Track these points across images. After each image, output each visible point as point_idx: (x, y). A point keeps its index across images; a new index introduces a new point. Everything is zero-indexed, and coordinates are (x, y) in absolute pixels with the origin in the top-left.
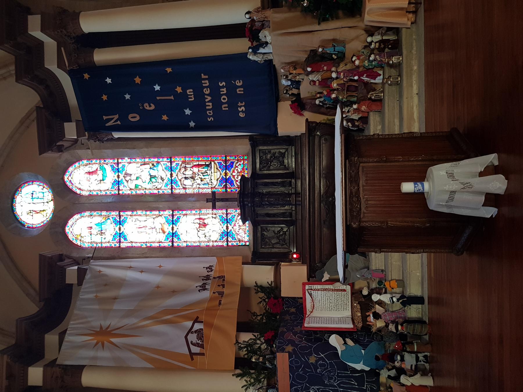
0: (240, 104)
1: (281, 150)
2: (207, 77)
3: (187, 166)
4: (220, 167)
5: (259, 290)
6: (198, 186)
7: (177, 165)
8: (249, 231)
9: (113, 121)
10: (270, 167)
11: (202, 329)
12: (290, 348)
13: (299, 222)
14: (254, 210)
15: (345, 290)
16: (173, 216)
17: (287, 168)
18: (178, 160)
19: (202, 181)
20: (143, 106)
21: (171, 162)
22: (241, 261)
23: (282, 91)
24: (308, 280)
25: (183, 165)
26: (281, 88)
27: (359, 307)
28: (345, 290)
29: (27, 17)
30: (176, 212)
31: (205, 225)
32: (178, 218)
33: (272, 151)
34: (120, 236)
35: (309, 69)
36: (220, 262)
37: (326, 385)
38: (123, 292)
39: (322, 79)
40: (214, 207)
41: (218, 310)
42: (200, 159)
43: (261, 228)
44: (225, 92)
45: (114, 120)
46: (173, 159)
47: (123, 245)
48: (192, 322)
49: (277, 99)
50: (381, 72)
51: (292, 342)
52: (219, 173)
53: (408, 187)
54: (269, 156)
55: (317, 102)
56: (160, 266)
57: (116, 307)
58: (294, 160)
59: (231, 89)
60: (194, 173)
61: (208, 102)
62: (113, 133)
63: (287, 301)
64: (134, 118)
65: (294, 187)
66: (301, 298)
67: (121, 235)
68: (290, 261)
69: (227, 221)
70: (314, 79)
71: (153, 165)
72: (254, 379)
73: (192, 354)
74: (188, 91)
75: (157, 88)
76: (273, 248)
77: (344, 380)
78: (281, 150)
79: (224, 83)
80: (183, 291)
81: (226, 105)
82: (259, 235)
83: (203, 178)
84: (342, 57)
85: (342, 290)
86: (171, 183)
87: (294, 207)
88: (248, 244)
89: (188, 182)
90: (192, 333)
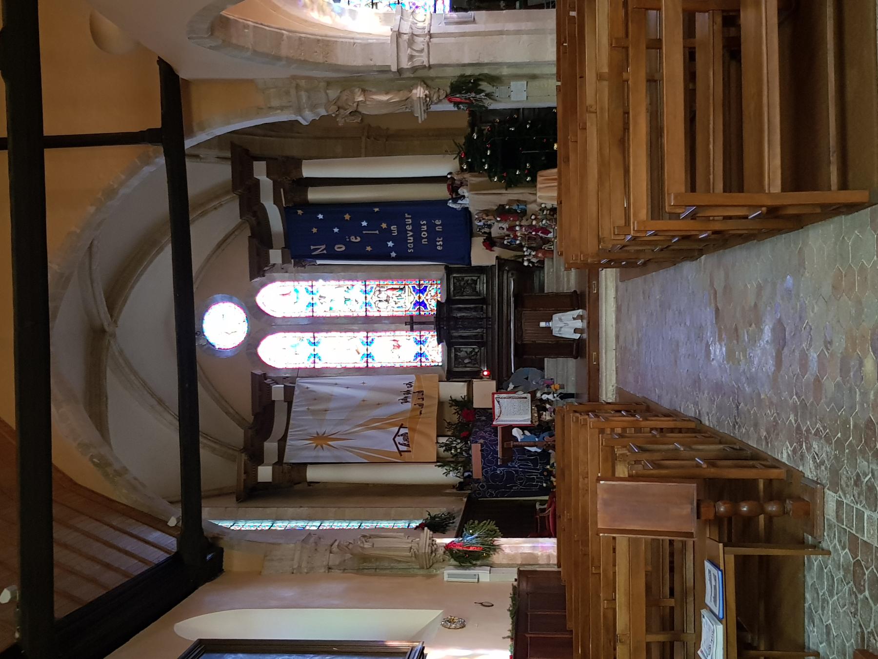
0: (438, 239)
1: (473, 278)
2: (410, 216)
3: (381, 289)
4: (414, 291)
5: (454, 403)
6: (393, 309)
7: (372, 288)
8: (443, 351)
9: (319, 251)
10: (463, 293)
11: (407, 433)
12: (482, 441)
13: (490, 343)
14: (449, 333)
15: (526, 398)
16: (367, 337)
17: (478, 294)
18: (372, 284)
19: (396, 304)
20: (349, 238)
21: (365, 285)
22: (437, 379)
23: (475, 230)
24: (497, 391)
25: (378, 289)
26: (475, 227)
27: (536, 409)
28: (526, 398)
29: (253, 163)
30: (370, 334)
31: (399, 347)
32: (373, 340)
33: (466, 278)
34: (314, 357)
35: (499, 219)
36: (418, 379)
37: (510, 467)
38: (331, 405)
39: (509, 227)
40: (412, 330)
41: (419, 418)
42: (395, 283)
43: (455, 348)
44: (426, 229)
45: (321, 249)
46: (367, 283)
47: (318, 366)
48: (398, 428)
49: (471, 235)
50: (552, 230)
51: (483, 438)
52: (412, 296)
53: (543, 324)
54: (462, 283)
55: (505, 242)
56: (364, 383)
57: (328, 417)
58: (485, 285)
59: (431, 228)
60: (388, 296)
61: (410, 236)
62: (317, 261)
63: (479, 411)
64: (340, 248)
65: (485, 312)
66: (491, 409)
67: (316, 356)
68: (481, 378)
69: (420, 343)
70: (503, 226)
71: (348, 288)
72: (453, 468)
73: (400, 452)
74: (392, 227)
75: (364, 224)
76: (466, 367)
77: (523, 463)
78: (473, 278)
79: (425, 222)
80: (387, 404)
81: (426, 240)
82: (453, 355)
83: (397, 301)
84: (524, 213)
85: (523, 398)
86: (366, 305)
87: (485, 330)
88: (440, 364)
89: (383, 305)
90: (399, 436)
